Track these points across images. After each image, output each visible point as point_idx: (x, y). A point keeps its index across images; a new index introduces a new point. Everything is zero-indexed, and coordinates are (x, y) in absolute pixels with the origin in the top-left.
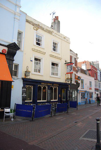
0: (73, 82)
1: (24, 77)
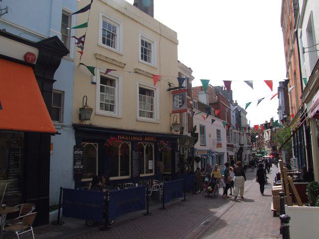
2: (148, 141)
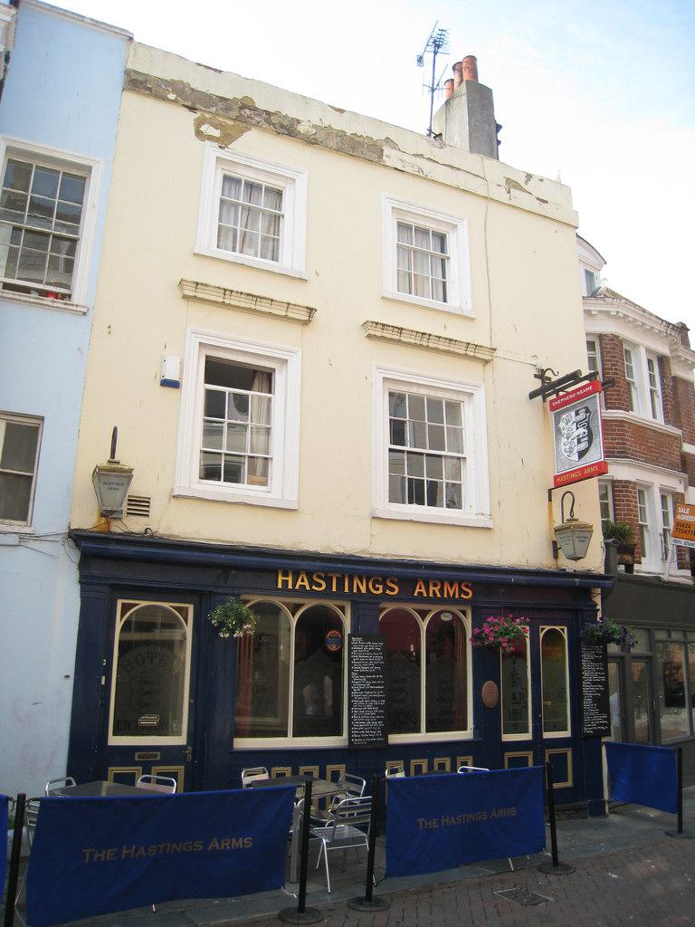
1: (87, 520)
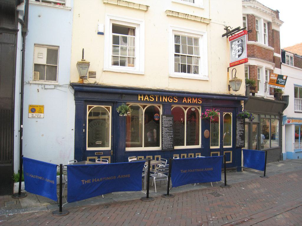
0: (263, 93)
1: (76, 80)
2: (189, 104)
